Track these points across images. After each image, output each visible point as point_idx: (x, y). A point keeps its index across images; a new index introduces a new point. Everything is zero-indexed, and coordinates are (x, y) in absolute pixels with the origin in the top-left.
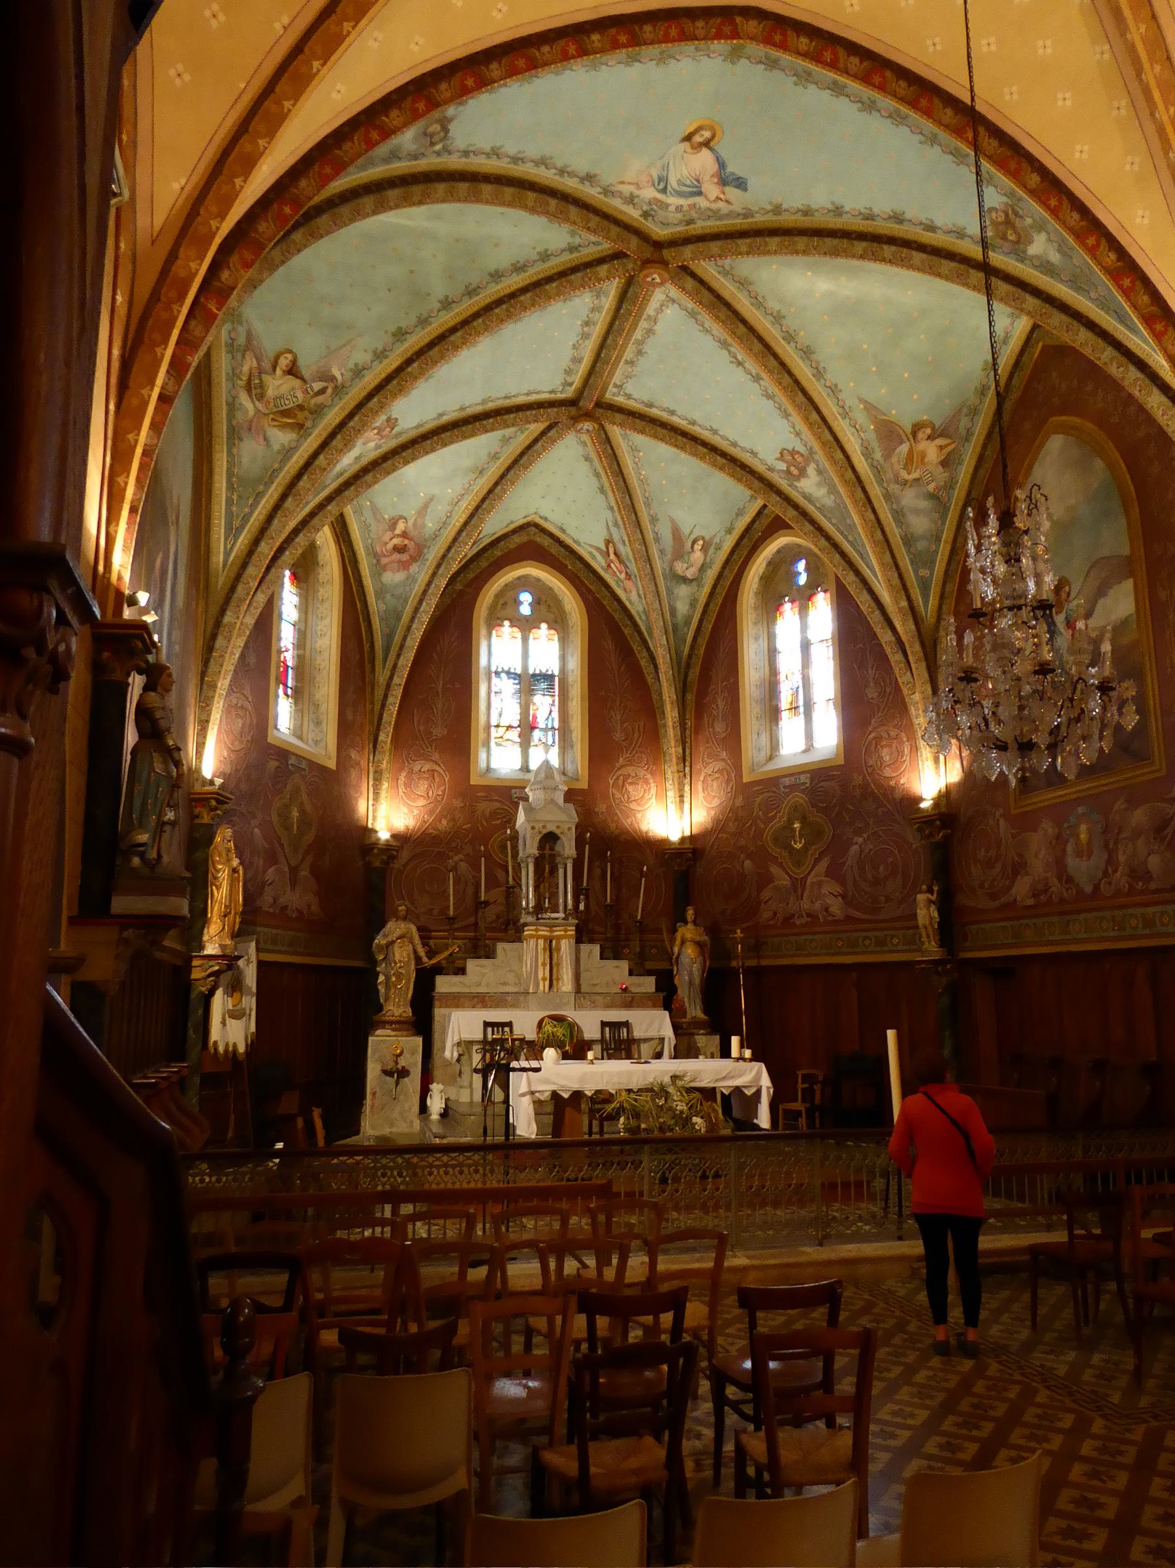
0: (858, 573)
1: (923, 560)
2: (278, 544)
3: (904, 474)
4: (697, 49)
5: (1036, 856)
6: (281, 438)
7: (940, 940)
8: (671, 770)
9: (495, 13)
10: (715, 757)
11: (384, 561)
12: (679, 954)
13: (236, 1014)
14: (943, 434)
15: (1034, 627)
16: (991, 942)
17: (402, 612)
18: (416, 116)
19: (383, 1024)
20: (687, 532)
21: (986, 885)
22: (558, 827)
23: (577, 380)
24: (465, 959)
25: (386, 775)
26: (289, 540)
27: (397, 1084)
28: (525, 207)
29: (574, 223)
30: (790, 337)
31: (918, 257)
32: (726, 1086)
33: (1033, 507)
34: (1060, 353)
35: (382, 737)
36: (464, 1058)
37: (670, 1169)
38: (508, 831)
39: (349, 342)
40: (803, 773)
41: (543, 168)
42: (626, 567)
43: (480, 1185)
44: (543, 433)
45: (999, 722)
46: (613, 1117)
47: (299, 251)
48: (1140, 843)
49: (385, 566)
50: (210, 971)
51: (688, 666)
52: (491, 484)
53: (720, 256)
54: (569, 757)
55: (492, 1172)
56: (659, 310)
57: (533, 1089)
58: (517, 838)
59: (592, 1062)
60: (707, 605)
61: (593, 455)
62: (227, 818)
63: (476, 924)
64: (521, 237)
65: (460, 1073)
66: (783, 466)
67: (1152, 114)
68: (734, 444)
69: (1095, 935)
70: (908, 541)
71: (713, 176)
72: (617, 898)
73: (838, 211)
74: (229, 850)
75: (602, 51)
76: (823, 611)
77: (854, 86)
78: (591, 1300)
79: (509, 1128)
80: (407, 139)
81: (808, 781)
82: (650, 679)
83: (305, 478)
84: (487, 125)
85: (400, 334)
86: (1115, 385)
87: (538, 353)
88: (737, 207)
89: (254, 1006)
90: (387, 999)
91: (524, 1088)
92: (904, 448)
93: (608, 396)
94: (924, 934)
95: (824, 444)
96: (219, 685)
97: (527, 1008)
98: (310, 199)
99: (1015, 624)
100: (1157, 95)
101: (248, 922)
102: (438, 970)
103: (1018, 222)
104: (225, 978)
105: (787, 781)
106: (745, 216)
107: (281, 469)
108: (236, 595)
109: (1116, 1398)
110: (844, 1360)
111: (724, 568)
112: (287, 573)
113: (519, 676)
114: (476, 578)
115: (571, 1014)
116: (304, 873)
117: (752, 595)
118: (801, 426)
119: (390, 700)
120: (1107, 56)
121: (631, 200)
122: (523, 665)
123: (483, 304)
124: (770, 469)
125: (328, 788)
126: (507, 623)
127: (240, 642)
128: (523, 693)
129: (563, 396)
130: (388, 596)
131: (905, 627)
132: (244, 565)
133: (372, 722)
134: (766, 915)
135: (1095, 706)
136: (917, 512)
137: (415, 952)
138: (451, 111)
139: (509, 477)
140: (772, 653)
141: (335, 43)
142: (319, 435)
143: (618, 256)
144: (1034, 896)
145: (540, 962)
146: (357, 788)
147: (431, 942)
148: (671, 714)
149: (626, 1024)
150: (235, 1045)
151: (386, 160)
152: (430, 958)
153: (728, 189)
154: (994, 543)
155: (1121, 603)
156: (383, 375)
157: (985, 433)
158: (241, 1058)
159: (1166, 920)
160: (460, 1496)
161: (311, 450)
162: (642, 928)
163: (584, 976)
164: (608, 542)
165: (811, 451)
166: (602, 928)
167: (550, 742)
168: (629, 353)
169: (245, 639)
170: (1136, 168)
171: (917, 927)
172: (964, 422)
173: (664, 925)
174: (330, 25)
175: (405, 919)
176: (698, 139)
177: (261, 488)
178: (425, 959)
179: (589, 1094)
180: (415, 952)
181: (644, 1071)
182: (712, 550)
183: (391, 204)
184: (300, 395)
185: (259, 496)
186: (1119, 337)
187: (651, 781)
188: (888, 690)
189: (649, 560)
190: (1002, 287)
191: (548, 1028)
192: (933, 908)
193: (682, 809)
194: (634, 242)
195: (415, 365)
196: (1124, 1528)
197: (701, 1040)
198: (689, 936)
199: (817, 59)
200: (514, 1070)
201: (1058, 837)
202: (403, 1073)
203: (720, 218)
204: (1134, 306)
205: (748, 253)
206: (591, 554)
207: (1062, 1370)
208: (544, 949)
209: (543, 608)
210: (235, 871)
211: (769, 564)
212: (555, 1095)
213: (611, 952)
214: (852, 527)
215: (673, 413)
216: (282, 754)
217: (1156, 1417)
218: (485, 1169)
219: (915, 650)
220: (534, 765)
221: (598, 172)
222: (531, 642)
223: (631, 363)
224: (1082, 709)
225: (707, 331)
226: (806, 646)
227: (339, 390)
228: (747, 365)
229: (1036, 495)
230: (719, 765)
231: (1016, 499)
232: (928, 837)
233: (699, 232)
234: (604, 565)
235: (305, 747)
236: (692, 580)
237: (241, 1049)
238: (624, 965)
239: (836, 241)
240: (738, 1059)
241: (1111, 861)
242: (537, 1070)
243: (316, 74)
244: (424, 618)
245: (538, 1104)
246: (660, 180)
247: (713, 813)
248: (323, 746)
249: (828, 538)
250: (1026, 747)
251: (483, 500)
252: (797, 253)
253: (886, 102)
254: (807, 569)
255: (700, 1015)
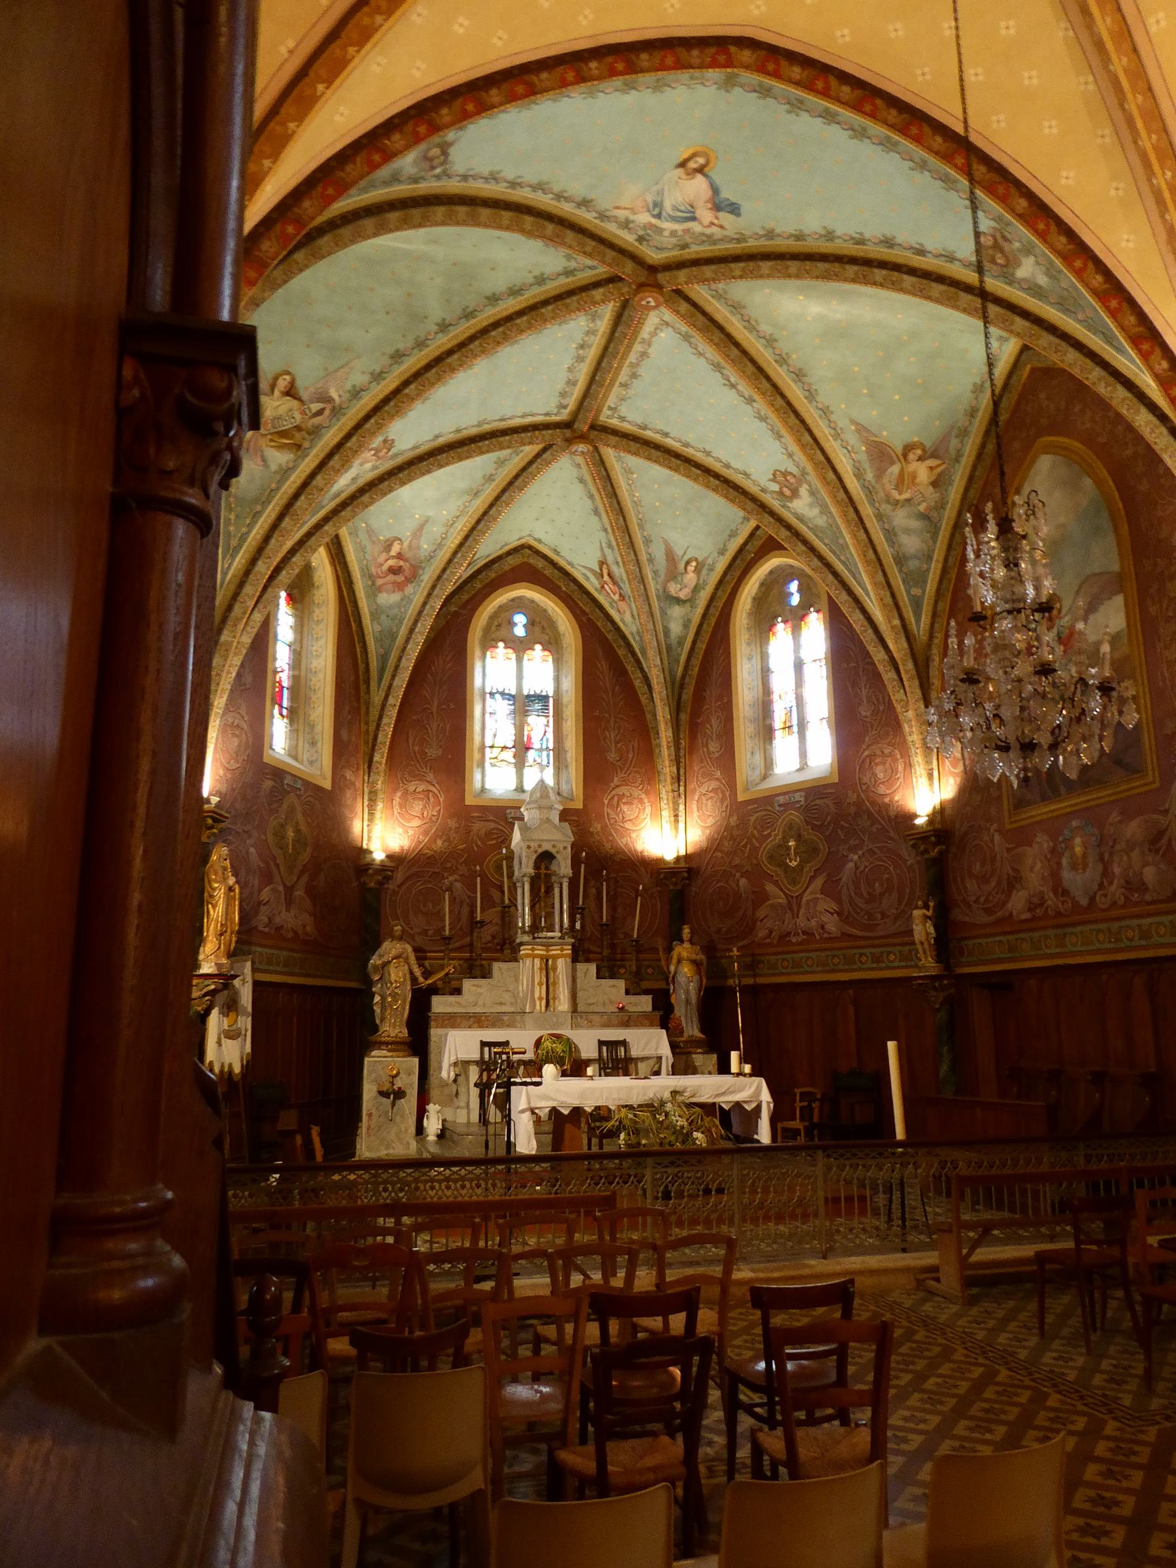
0: (850, 592)
1: (915, 579)
2: (275, 564)
3: (895, 494)
4: (692, 78)
5: (1032, 870)
6: (278, 458)
7: (938, 956)
8: (665, 790)
9: (495, 40)
10: (710, 776)
11: (379, 582)
12: (676, 972)
13: (232, 1034)
14: (934, 455)
15: (1034, 630)
16: (988, 956)
17: (398, 631)
18: (417, 140)
19: (379, 1045)
20: (680, 553)
21: (982, 899)
22: (554, 846)
23: (572, 402)
24: (461, 980)
25: (381, 796)
26: (285, 560)
27: (393, 1105)
28: (522, 231)
29: (570, 247)
30: (782, 360)
31: (909, 280)
32: (726, 1101)
33: (1032, 512)
34: (1048, 375)
35: (377, 758)
36: (460, 1079)
37: (673, 1182)
38: (504, 851)
39: (347, 364)
40: (799, 790)
41: (540, 193)
42: (620, 588)
43: (482, 1198)
44: (538, 455)
45: (1002, 722)
46: (613, 1134)
47: (301, 271)
48: (1135, 855)
49: (380, 586)
50: (205, 990)
51: (682, 686)
52: (486, 506)
53: (714, 280)
54: (564, 776)
55: (494, 1185)
56: (654, 334)
57: (533, 1105)
58: (513, 859)
59: (591, 1077)
60: (701, 625)
61: (588, 478)
62: (223, 836)
63: (471, 944)
64: (517, 260)
65: (457, 1094)
66: (775, 487)
67: (1135, 142)
68: (728, 466)
69: (1092, 947)
70: (900, 560)
71: (707, 202)
72: (613, 917)
73: (830, 235)
74: (225, 869)
75: (600, 78)
76: (815, 628)
77: (846, 114)
78: (604, 1304)
79: (510, 1145)
80: (408, 162)
81: (802, 799)
82: (643, 699)
83: (303, 497)
84: (486, 150)
85: (398, 356)
86: (1103, 405)
87: (532, 376)
88: (730, 232)
89: (249, 1027)
90: (382, 1020)
91: (523, 1105)
92: (895, 469)
93: (603, 418)
94: (921, 951)
95: (817, 465)
96: (216, 703)
97: (523, 1028)
98: (313, 219)
99: (1015, 627)
100: (1140, 124)
101: (245, 940)
102: (434, 990)
103: (1006, 246)
104: (221, 998)
105: (781, 799)
106: (739, 241)
107: (278, 489)
108: (233, 614)
109: (1127, 1401)
110: (862, 1356)
111: (717, 589)
112: (283, 594)
113: (514, 696)
114: (472, 598)
115: (567, 1032)
116: (299, 893)
117: (745, 615)
118: (794, 447)
119: (385, 720)
120: (1091, 87)
121: (626, 225)
122: (517, 688)
123: (479, 327)
124: (763, 490)
125: (323, 807)
126: (501, 644)
127: (237, 661)
128: (518, 718)
129: (558, 418)
130: (383, 617)
131: (898, 646)
132: (241, 584)
133: (366, 743)
134: (762, 933)
135: (1095, 704)
136: (907, 531)
137: (411, 973)
138: (451, 135)
139: (504, 498)
140: (765, 672)
141: (340, 66)
142: (317, 456)
143: (613, 280)
144: (1030, 910)
145: (537, 981)
146: (353, 810)
147: (427, 963)
148: (665, 734)
149: (624, 1043)
150: (230, 1065)
151: (387, 183)
152: (426, 979)
153: (721, 214)
154: (994, 548)
155: (1113, 617)
156: (381, 396)
157: (974, 453)
158: (236, 1079)
159: (1162, 930)
160: (477, 1495)
161: (308, 471)
162: (639, 948)
163: (580, 994)
164: (602, 563)
165: (804, 473)
166: (600, 947)
167: (545, 762)
168: (623, 377)
169: (241, 657)
170: (1121, 193)
171: (913, 943)
172: (954, 443)
173: (660, 943)
174: (335, 49)
175: (401, 939)
176: (692, 165)
177: (259, 508)
178: (421, 979)
179: (589, 1110)
180: (411, 973)
181: (644, 1087)
182: (704, 572)
183: (392, 226)
184: (298, 416)
185: (256, 515)
186: (1107, 358)
187: (646, 801)
188: (881, 708)
189: (643, 580)
190: (993, 309)
191: (547, 1044)
192: (929, 924)
193: (676, 829)
194: (629, 267)
195: (412, 386)
196: (1141, 1524)
197: (698, 1059)
198: (685, 954)
199: (809, 87)
200: (515, 1084)
201: (1053, 851)
202: (400, 1094)
203: (714, 243)
204: (1123, 328)
205: (741, 277)
206: (585, 575)
207: (1072, 1376)
208: (541, 969)
209: (537, 629)
210: (231, 889)
211: (762, 584)
212: (554, 1111)
213: (607, 971)
214: (844, 547)
215: (666, 435)
216: (278, 773)
217: (1168, 1418)
218: (487, 1184)
219: (907, 667)
220: (529, 785)
221: (593, 196)
222: (525, 662)
223: (624, 385)
224: (1083, 709)
225: (701, 354)
226: (799, 666)
227: (337, 411)
228: (740, 387)
229: (1034, 500)
230: (714, 784)
231: (1014, 504)
232: (922, 853)
233: (694, 256)
234: (598, 586)
235: (301, 767)
236: (685, 602)
237: (237, 1069)
238: (621, 984)
239: (827, 265)
240: (738, 1075)
241: (1106, 873)
242: (538, 1084)
243: (321, 96)
244: (419, 639)
245: (538, 1121)
246: (656, 205)
247: (708, 832)
248: (318, 766)
249: (821, 558)
250: (1028, 747)
251: (479, 521)
252: (790, 276)
253: (877, 130)
254: (800, 590)
255: (697, 1033)
